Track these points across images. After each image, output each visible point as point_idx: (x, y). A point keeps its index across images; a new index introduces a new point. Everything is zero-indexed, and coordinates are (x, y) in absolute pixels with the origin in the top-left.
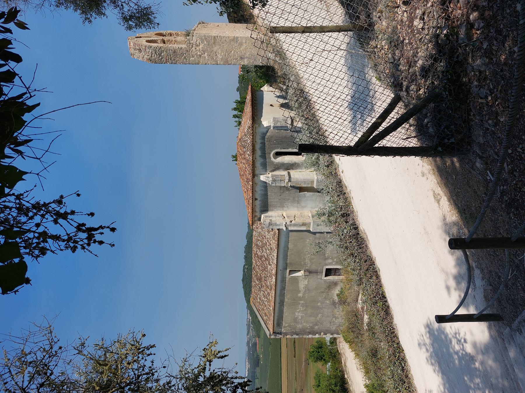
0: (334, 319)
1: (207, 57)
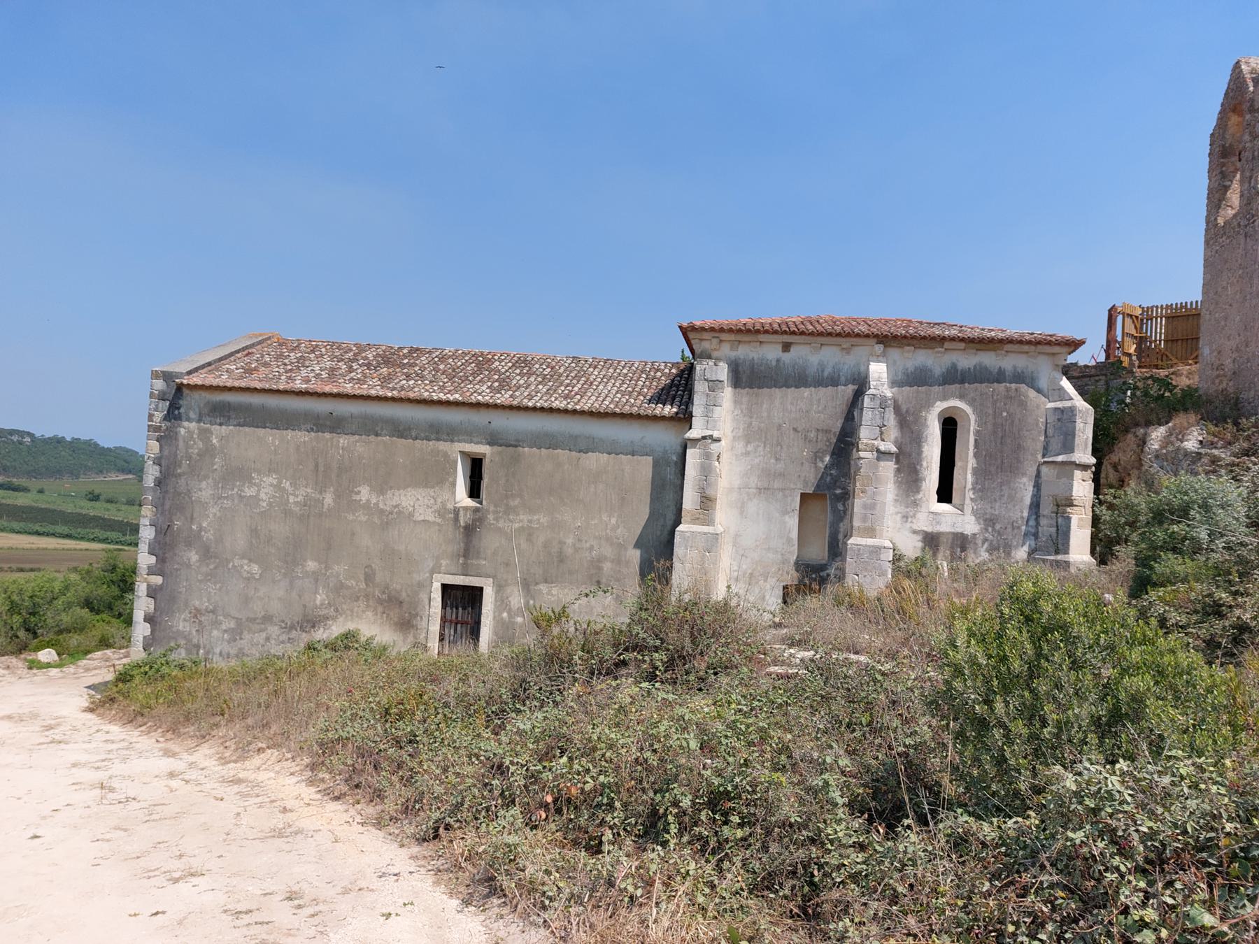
0: (229, 624)
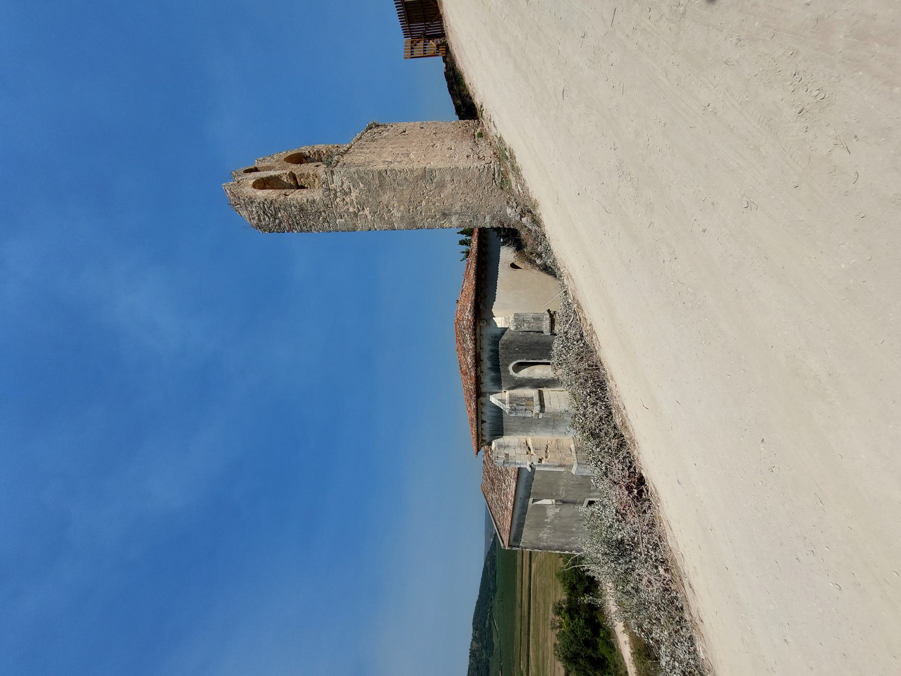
1: (369, 217)
